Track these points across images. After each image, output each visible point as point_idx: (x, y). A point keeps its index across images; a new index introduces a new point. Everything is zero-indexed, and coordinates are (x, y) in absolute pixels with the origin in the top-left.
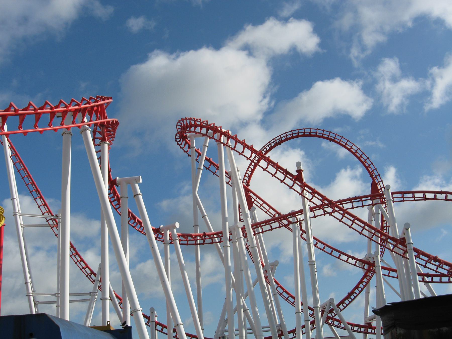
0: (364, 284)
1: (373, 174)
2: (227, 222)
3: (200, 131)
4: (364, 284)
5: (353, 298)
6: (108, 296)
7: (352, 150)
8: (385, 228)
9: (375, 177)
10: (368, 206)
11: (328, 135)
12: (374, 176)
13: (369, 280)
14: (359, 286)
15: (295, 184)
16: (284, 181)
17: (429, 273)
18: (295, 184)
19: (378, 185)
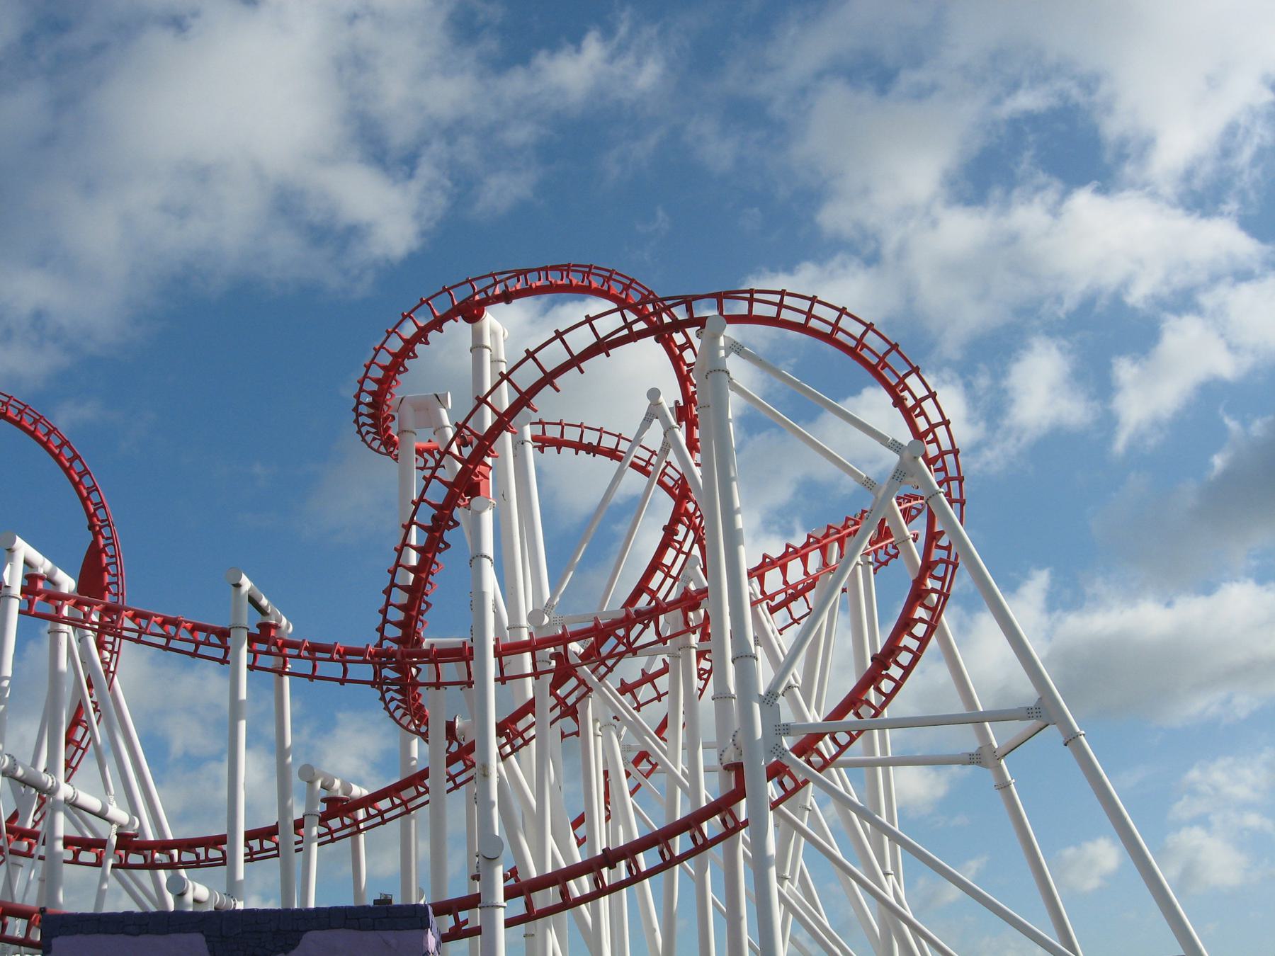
0: (920, 630)
1: (906, 394)
2: (241, 719)
3: (401, 718)
4: (920, 630)
5: (917, 646)
6: (494, 796)
7: (840, 336)
8: (373, 812)
9: (914, 408)
10: (472, 418)
11: (647, 460)
12: (910, 402)
13: (936, 612)
14: (901, 645)
15: (347, 664)
16: (348, 677)
17: (633, 343)
18: (347, 664)
19: (917, 416)
